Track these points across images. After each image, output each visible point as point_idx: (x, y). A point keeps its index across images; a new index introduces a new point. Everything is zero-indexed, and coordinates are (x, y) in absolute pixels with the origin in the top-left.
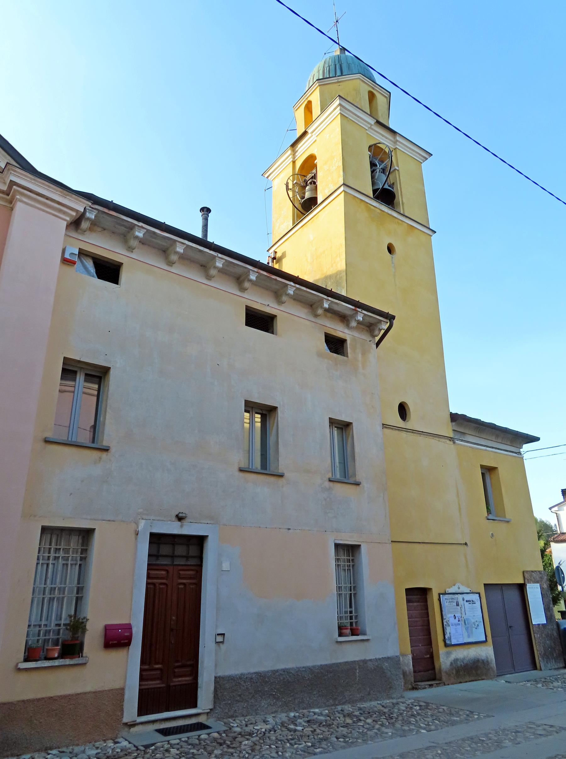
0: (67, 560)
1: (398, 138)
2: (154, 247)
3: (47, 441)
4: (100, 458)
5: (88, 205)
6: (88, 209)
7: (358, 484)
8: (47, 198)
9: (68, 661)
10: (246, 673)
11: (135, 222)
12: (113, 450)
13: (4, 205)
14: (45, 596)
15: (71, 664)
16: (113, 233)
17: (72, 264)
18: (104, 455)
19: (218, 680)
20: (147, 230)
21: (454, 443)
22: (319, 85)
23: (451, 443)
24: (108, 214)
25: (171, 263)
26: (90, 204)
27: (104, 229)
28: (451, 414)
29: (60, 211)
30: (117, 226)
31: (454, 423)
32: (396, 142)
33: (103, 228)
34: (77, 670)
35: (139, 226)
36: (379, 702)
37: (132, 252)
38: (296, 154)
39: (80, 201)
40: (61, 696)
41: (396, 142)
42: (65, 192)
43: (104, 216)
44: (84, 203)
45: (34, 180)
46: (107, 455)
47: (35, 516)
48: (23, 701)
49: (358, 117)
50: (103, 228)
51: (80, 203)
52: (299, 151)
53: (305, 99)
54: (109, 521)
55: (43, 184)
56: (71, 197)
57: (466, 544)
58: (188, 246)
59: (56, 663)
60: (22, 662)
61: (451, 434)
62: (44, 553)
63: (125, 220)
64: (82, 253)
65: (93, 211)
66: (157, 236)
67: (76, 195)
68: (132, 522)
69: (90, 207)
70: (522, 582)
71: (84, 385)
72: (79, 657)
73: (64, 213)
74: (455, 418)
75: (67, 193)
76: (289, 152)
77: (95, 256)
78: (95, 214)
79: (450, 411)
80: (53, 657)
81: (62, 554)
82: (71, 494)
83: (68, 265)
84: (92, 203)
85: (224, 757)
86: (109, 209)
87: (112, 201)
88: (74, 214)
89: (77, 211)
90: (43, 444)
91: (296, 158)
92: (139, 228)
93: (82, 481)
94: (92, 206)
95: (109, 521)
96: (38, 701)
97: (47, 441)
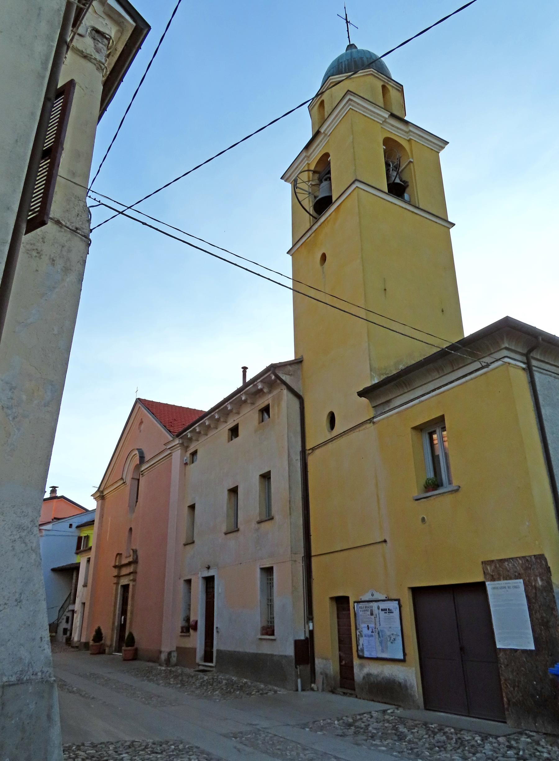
11: (239, 395)
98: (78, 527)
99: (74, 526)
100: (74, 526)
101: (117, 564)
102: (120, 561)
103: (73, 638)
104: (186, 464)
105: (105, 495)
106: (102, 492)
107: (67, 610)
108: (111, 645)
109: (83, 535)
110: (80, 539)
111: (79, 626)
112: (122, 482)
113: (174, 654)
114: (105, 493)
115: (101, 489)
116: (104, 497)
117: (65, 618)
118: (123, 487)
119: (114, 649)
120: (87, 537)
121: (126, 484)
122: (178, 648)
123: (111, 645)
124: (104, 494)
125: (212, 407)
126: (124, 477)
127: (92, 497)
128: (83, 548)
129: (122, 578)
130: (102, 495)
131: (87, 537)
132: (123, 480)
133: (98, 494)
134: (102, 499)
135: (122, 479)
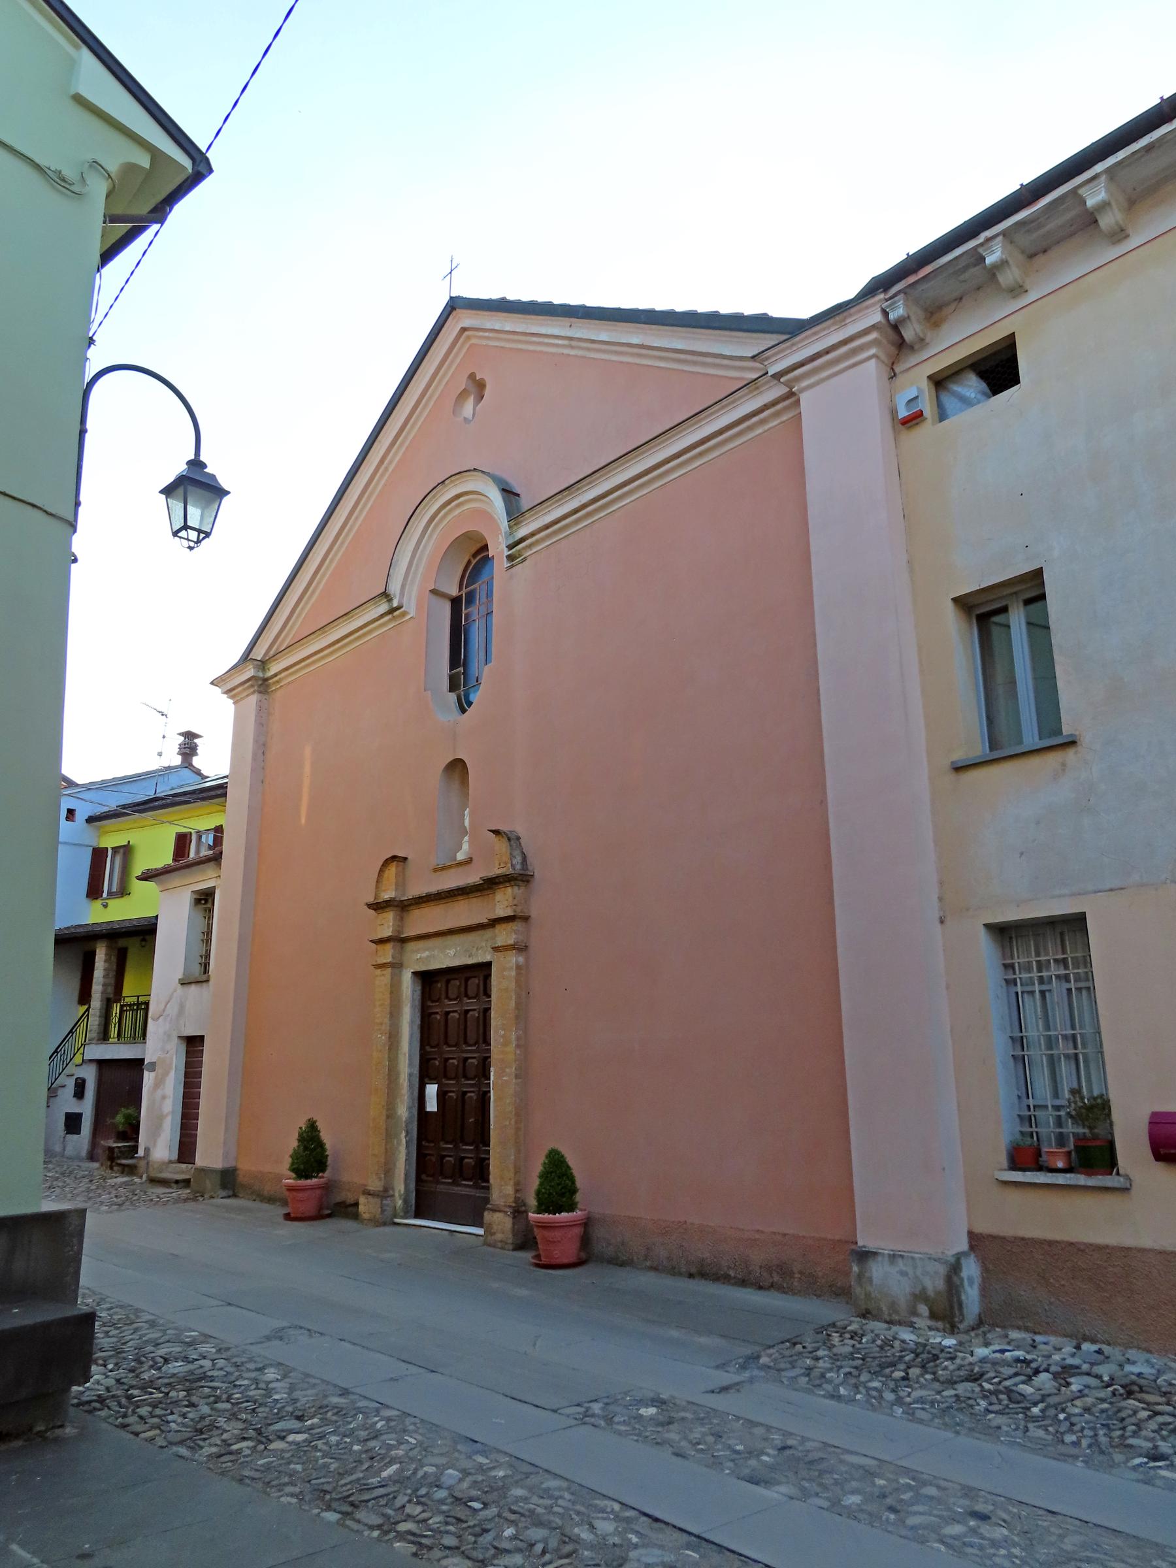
0: (1068, 980)
2: (1071, 235)
3: (959, 769)
4: (1064, 765)
5: (880, 300)
6: (887, 307)
8: (827, 351)
9: (1081, 1179)
10: (345, 1177)
11: (972, 244)
12: (1086, 739)
13: (792, 417)
14: (1054, 1052)
15: (1079, 1184)
16: (978, 289)
17: (918, 420)
18: (1070, 753)
20: (1004, 233)
24: (919, 280)
25: (1119, 235)
26: (882, 296)
27: (961, 299)
29: (854, 352)
30: (962, 277)
33: (956, 300)
34: (1110, 1200)
35: (982, 245)
36: (1171, 1426)
37: (1027, 291)
39: (867, 308)
40: (1091, 1245)
42: (837, 318)
43: (921, 287)
44: (873, 305)
45: (793, 345)
46: (1076, 753)
47: (968, 910)
48: (1023, 1239)
50: (956, 300)
51: (870, 310)
54: (1111, 890)
55: (806, 338)
56: (851, 315)
58: (1108, 171)
59: (1060, 1179)
60: (1005, 1170)
62: (1020, 973)
63: (950, 261)
64: (940, 382)
65: (895, 302)
66: (1032, 222)
67: (839, 314)
68: (1168, 881)
69: (887, 300)
71: (200, 837)
72: (1111, 1174)
73: (861, 348)
75: (841, 316)
77: (970, 362)
78: (901, 302)
80: (1054, 1167)
81: (1055, 970)
82: (1022, 854)
83: (917, 424)
84: (881, 292)
86: (915, 271)
88: (874, 335)
89: (874, 327)
90: (952, 776)
92: (986, 246)
93: (1038, 823)
94: (887, 297)
95: (1111, 890)
97: (959, 769)
98: (91, 820)
99: (81, 816)
100: (81, 816)
101: (386, 896)
102: (401, 884)
103: (147, 1150)
104: (915, 419)
105: (275, 675)
106: (263, 664)
107: (78, 1059)
108: (386, 1190)
109: (110, 841)
110: (99, 855)
111: (173, 1112)
112: (384, 607)
113: (971, 1269)
114: (274, 668)
115: (258, 653)
116: (268, 686)
117: (71, 1084)
118: (388, 625)
119: (400, 1203)
120: (122, 851)
121: (404, 614)
122: (976, 1240)
123: (385, 1193)
124: (269, 674)
125: (1026, 181)
126: (395, 588)
127: (217, 690)
128: (198, 851)
129: (411, 946)
130: (261, 674)
131: (122, 851)
132: (390, 600)
133: (250, 672)
134: (260, 692)
135: (386, 595)
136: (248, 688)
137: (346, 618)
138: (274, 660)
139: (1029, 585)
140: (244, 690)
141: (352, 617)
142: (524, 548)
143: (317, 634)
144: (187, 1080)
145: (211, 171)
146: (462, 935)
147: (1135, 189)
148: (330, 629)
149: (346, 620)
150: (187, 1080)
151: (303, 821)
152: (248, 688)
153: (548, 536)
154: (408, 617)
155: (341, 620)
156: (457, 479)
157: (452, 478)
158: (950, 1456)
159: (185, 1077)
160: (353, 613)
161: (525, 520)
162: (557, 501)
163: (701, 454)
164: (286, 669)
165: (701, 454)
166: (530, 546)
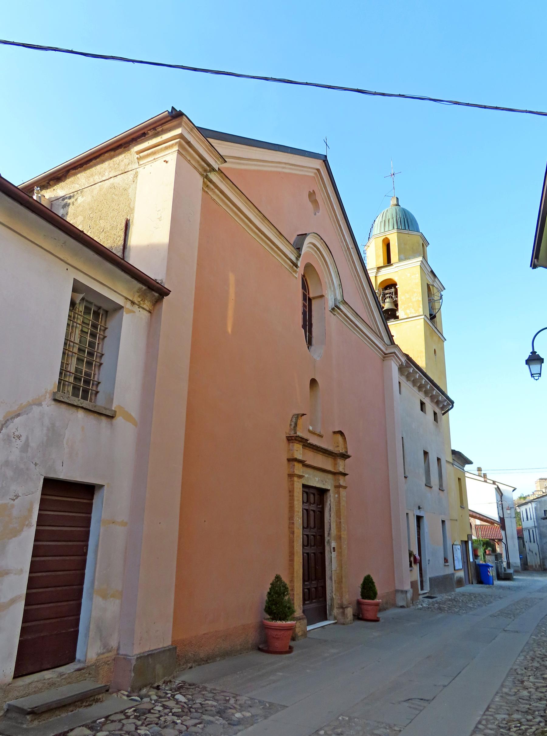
1: (436, 280)
7: (431, 487)
19: (431, 579)
21: (453, 466)
22: (397, 232)
23: (452, 466)
28: (452, 450)
31: (453, 455)
32: (434, 281)
38: (379, 273)
41: (434, 281)
49: (426, 267)
52: (381, 272)
53: (384, 235)
57: (457, 520)
61: (451, 461)
70: (467, 540)
74: (454, 452)
76: (376, 270)
79: (452, 449)
85: (112, 647)
87: (393, 336)
91: (378, 275)
96: (322, 587)
136: (203, 167)
137: (278, 234)
138: (222, 177)
139: (128, 657)
140: (198, 162)
141: (280, 238)
142: (338, 312)
143: (260, 214)
144: (41, 528)
145: (452, 403)
146: (312, 469)
147: (54, 190)
148: (266, 224)
149: (276, 234)
150: (41, 528)
151: (230, 330)
152: (203, 167)
153: (343, 318)
154: (294, 274)
155: (276, 231)
156: (324, 245)
157: (324, 243)
158: (393, 619)
159: (91, 505)
160: (283, 238)
161: (345, 305)
162: (353, 313)
163: (371, 344)
164: (222, 192)
165: (371, 344)
166: (339, 313)
